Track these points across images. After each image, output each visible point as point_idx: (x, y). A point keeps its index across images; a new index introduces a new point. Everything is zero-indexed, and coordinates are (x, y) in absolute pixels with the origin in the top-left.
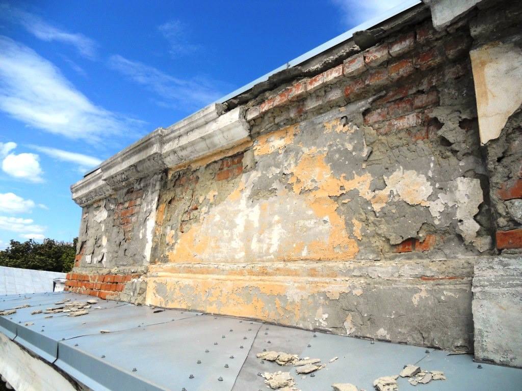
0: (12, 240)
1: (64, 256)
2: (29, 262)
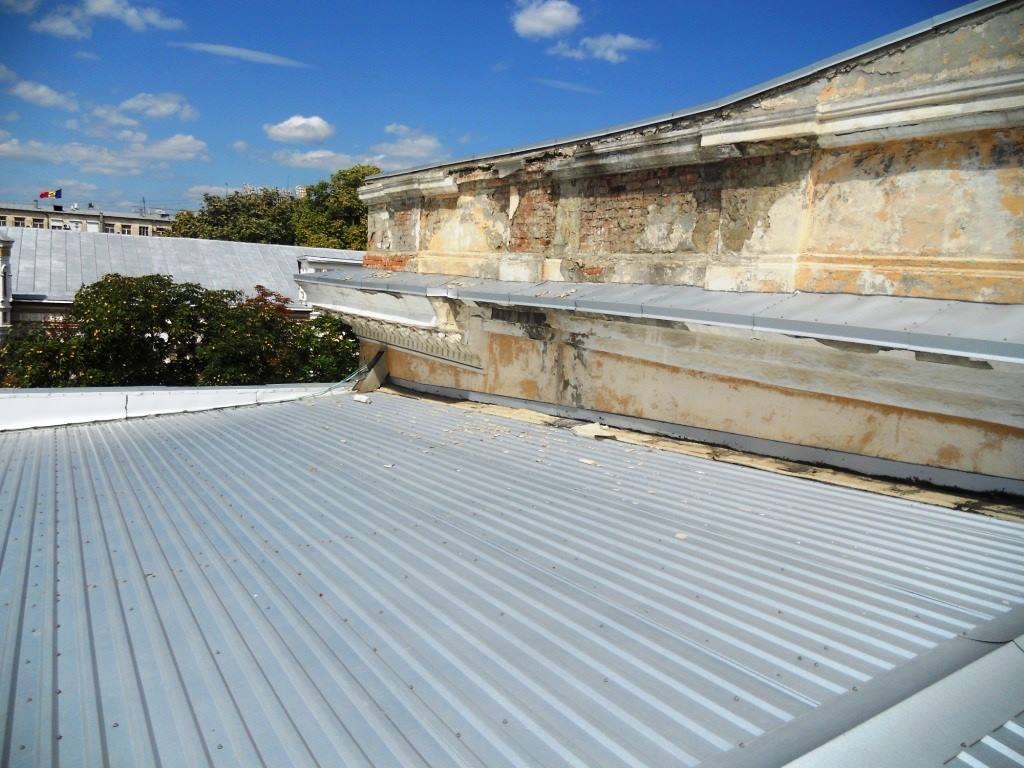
0: (206, 195)
1: (295, 216)
2: (242, 228)
